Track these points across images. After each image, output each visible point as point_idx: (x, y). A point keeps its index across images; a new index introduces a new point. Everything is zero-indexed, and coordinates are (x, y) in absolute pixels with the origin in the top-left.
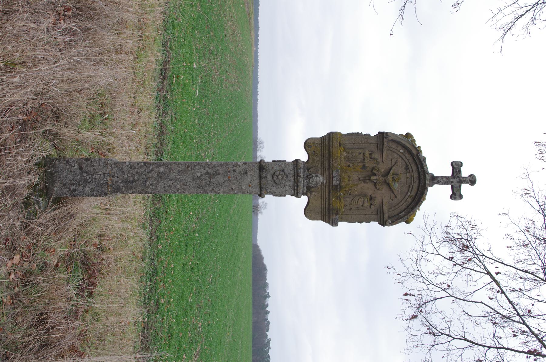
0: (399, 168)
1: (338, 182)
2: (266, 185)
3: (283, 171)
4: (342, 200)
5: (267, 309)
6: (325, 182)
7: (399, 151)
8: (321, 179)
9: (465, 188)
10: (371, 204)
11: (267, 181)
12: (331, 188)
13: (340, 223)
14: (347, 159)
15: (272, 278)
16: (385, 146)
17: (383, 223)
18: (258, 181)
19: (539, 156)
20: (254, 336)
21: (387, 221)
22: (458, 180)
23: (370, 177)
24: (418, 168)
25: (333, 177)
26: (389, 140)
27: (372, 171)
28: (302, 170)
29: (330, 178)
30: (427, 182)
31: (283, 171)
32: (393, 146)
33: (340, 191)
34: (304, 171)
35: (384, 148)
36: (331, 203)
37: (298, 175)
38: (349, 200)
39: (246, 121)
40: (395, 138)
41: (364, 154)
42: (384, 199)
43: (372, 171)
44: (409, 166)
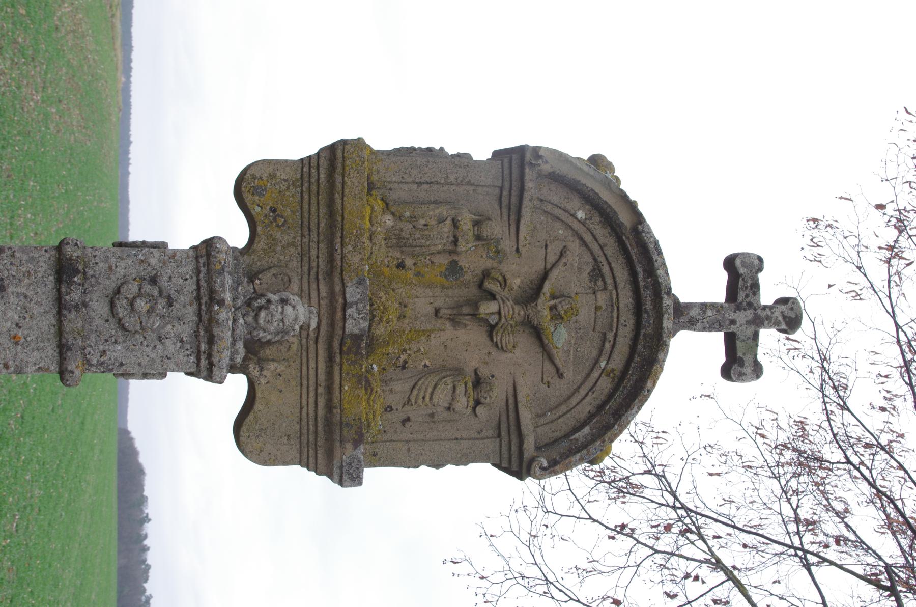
0: (569, 278)
1: (365, 325)
2: (85, 338)
3: (154, 281)
4: (377, 387)
5: (146, 542)
6: (314, 325)
7: (574, 216)
8: (299, 313)
9: (769, 339)
10: (478, 403)
11: (89, 320)
12: (336, 344)
13: (369, 473)
14: (397, 240)
15: (151, 487)
16: (527, 196)
17: (519, 468)
18: (51, 319)
19: (809, 253)
20: (120, 592)
21: (532, 460)
22: (749, 314)
23: (475, 304)
24: (633, 274)
25: (345, 306)
26: (540, 175)
27: (480, 285)
28: (228, 279)
29: (335, 308)
30: (667, 324)
31: (154, 281)
32: (556, 195)
33: (368, 355)
34: (239, 283)
35: (526, 202)
36: (336, 401)
37: (214, 299)
38: (401, 387)
39: (103, 205)
40: (564, 170)
41: (455, 223)
42: (520, 382)
43: (480, 285)
44: (606, 269)
